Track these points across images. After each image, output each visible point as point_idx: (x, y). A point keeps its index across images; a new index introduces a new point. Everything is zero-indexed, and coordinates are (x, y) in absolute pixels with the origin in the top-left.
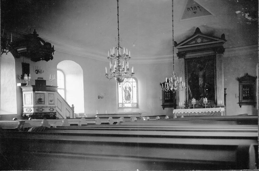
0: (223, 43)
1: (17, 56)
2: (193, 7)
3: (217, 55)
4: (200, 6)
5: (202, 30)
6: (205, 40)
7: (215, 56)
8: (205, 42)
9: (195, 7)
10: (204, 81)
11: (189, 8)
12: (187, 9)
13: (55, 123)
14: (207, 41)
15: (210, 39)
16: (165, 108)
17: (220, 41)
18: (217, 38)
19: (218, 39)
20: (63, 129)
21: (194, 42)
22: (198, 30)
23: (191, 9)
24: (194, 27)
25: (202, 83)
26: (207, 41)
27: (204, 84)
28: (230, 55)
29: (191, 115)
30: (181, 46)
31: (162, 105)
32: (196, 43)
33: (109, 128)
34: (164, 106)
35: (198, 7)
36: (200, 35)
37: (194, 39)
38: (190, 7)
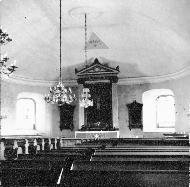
0: (117, 73)
1: (4, 143)
2: (94, 41)
3: (113, 83)
4: (100, 41)
5: (101, 61)
6: (102, 70)
7: (111, 84)
8: (102, 72)
9: (97, 41)
10: (101, 106)
11: (91, 41)
12: (89, 42)
13: (108, 159)
14: (104, 71)
15: (108, 69)
16: (63, 130)
17: (116, 72)
18: (113, 69)
19: (113, 70)
20: (126, 151)
21: (92, 71)
22: (96, 61)
23: (93, 42)
24: (93, 58)
25: (100, 107)
26: (104, 71)
27: (101, 108)
28: (35, 141)
29: (72, 143)
30: (82, 73)
31: (59, 127)
32: (94, 72)
33: (167, 150)
34: (62, 128)
35: (99, 41)
36: (98, 65)
37: (93, 69)
38: (92, 40)
